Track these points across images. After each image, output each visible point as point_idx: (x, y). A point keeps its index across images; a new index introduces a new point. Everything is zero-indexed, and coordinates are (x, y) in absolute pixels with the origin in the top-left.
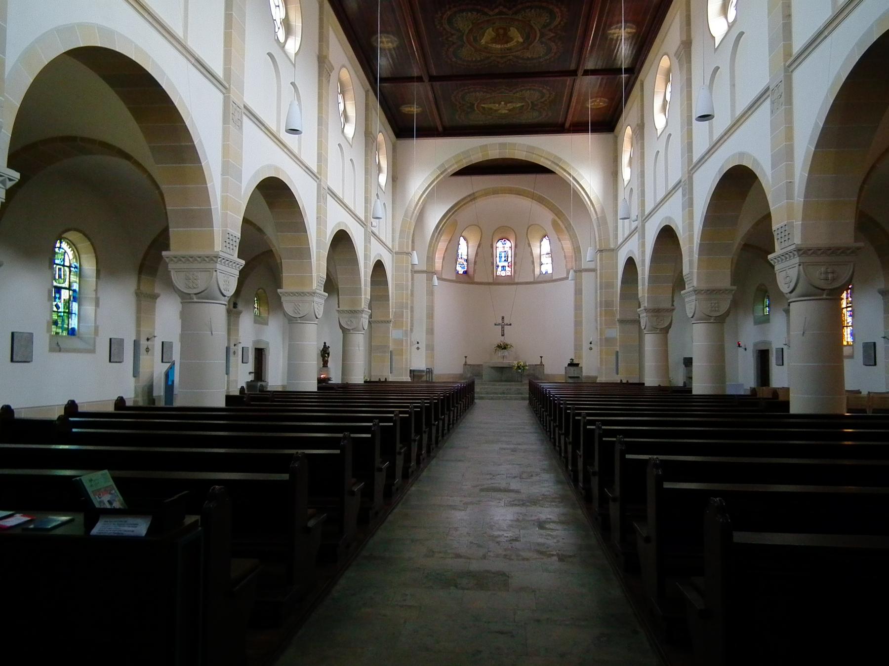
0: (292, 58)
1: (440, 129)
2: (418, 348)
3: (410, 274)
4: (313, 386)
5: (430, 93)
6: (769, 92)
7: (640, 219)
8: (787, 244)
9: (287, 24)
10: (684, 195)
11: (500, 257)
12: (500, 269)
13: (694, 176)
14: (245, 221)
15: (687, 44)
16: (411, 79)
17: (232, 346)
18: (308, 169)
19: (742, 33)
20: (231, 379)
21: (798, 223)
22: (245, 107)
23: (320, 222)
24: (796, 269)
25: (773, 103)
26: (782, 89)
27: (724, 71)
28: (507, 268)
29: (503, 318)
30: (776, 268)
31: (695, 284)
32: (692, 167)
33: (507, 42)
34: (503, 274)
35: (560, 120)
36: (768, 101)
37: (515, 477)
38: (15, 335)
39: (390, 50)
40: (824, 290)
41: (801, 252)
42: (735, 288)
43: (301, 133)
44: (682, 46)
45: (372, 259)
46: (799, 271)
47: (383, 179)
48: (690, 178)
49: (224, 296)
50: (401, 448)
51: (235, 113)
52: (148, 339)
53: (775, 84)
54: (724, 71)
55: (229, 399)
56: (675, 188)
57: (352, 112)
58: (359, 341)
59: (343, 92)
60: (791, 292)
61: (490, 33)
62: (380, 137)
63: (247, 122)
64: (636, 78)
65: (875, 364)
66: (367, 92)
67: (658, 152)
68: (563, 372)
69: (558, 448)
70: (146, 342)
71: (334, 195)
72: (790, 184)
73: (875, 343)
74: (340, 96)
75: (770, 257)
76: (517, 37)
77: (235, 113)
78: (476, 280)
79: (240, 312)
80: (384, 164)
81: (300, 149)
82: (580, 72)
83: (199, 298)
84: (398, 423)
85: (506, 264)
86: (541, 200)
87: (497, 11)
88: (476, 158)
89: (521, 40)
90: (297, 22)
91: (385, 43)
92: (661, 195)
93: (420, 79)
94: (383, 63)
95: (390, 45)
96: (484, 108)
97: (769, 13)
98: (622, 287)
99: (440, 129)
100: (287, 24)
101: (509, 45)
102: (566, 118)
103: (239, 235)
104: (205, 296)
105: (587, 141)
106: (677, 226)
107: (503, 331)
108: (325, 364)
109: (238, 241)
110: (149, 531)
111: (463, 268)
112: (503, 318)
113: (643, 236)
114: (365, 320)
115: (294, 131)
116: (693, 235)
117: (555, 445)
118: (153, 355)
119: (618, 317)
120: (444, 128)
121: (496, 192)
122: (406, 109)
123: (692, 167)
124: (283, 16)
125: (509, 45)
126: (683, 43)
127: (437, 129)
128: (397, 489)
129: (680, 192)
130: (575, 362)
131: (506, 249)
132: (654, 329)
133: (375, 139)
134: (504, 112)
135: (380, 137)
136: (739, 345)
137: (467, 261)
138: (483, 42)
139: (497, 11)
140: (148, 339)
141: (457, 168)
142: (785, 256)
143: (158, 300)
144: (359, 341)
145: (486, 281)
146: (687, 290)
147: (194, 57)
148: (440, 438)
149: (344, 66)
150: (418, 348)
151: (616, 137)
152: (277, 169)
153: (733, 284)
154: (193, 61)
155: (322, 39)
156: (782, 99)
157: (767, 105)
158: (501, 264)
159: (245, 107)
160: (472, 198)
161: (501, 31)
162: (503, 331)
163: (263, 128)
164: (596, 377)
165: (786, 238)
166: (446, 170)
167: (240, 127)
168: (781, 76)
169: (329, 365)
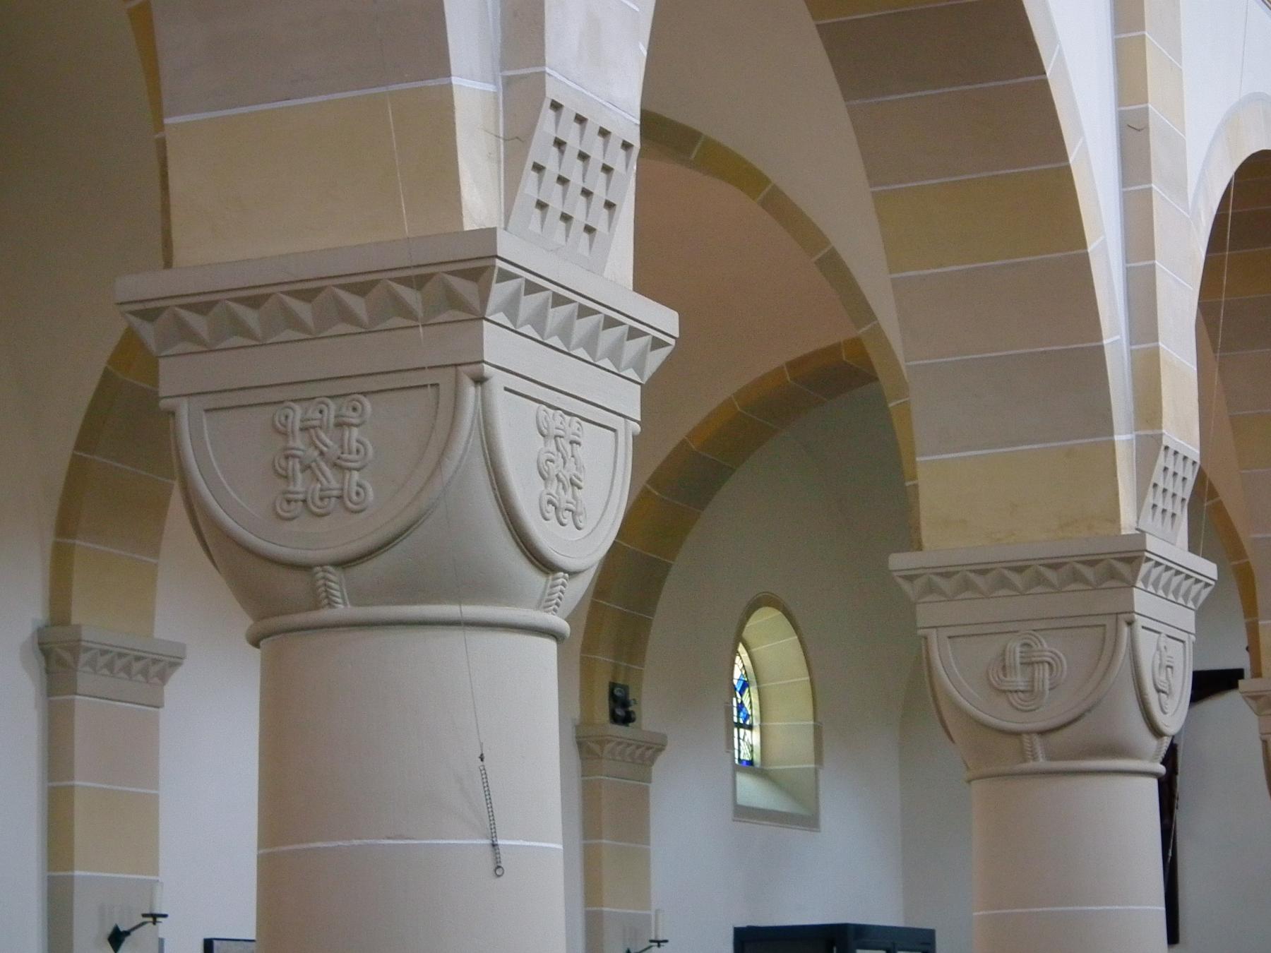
79: (653, 748)
104: (1083, 745)
143: (659, 768)
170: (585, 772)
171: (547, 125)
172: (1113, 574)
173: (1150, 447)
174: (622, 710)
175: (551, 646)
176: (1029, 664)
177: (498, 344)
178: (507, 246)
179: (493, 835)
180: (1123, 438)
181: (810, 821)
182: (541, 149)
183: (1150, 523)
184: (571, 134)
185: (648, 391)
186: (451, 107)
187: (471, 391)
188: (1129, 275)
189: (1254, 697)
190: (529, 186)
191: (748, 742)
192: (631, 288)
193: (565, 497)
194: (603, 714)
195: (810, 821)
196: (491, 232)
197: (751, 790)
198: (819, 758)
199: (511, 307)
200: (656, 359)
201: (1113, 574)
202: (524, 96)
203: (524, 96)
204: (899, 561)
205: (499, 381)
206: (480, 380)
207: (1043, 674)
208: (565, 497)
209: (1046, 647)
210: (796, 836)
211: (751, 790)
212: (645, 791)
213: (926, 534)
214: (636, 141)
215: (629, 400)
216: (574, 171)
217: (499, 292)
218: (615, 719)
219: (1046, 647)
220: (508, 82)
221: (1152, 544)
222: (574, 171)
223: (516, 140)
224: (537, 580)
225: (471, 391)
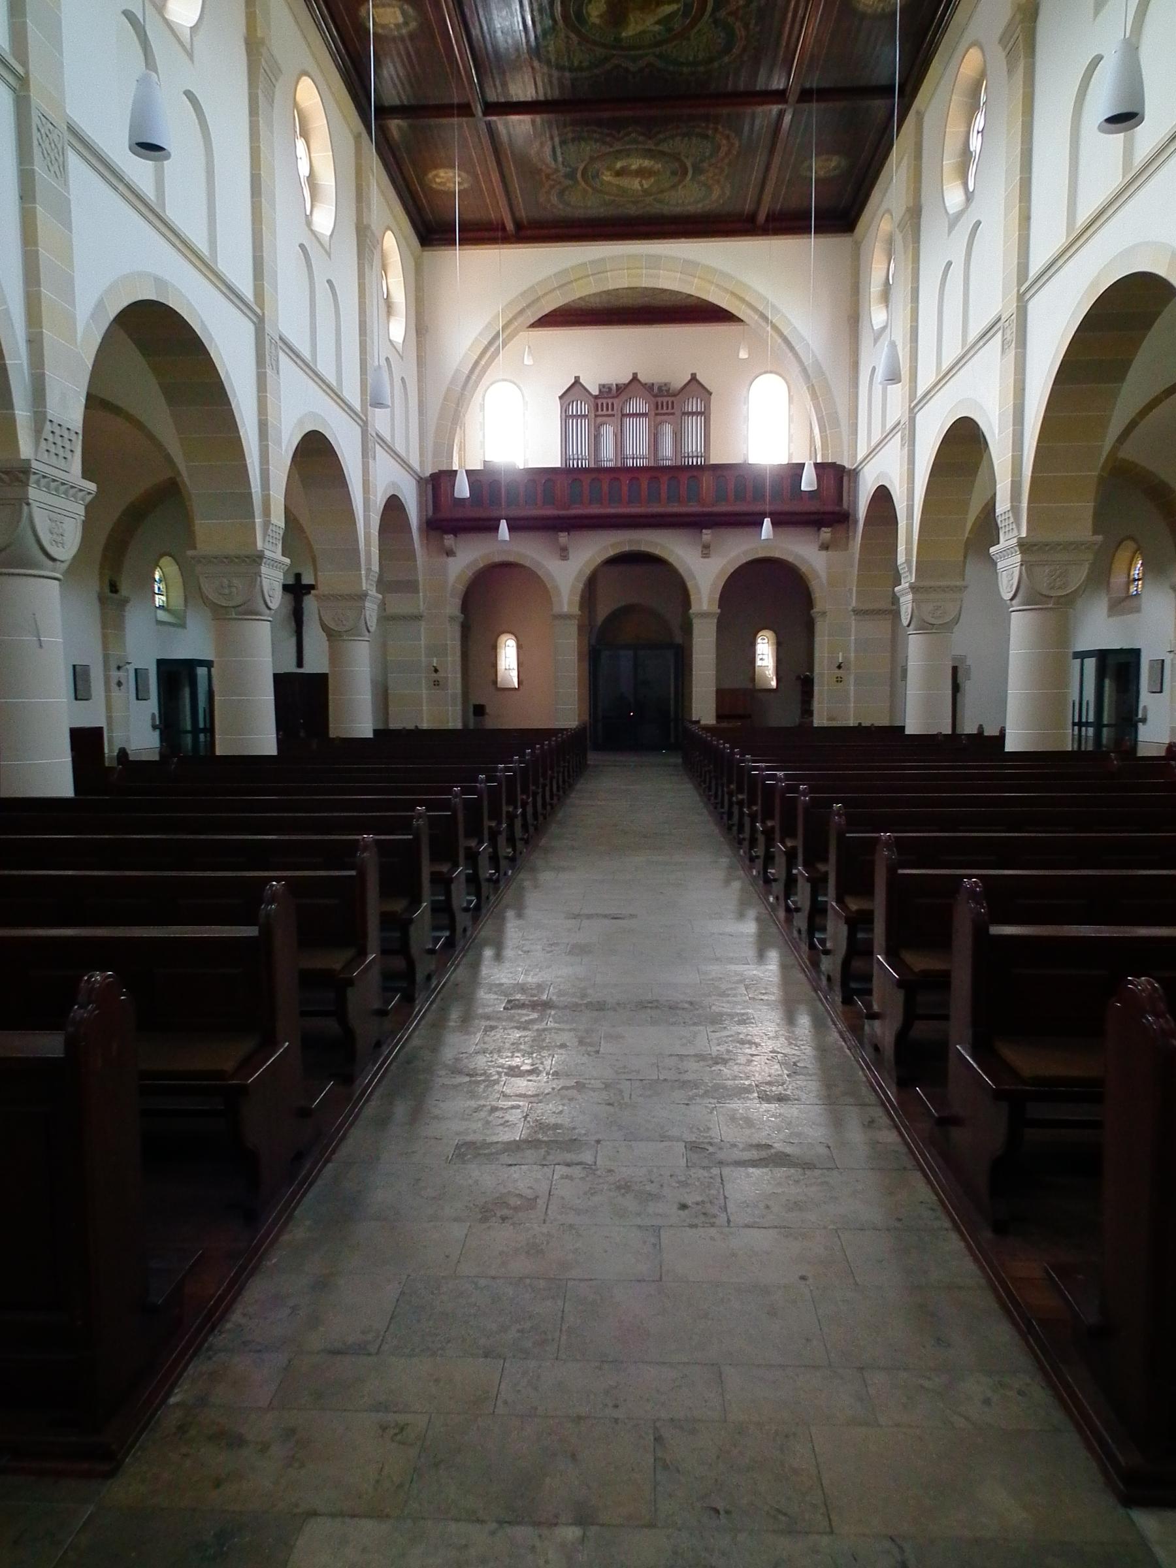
1: (510, 226)
4: (55, 777)
14: (90, 397)
15: (915, 213)
22: (281, 338)
23: (273, 411)
27: (957, 271)
30: (999, 565)
31: (854, 604)
32: (1026, 285)
35: (748, 207)
38: (78, 668)
42: (1100, 538)
43: (168, 157)
45: (379, 495)
47: (398, 329)
48: (912, 420)
49: (269, 609)
51: (267, 347)
52: (119, 668)
54: (957, 271)
56: (986, 335)
57: (327, 178)
59: (305, 135)
60: (1012, 599)
62: (390, 242)
66: (357, 138)
74: (300, 144)
75: (992, 550)
77: (267, 347)
79: (125, 602)
80: (399, 297)
81: (393, 436)
83: (240, 614)
92: (951, 353)
94: (389, 79)
99: (510, 226)
102: (759, 202)
103: (283, 526)
104: (247, 611)
105: (803, 252)
109: (282, 532)
113: (911, 441)
114: (371, 610)
115: (149, 148)
116: (913, 505)
119: (854, 604)
120: (519, 226)
123: (1026, 285)
126: (908, 210)
127: (504, 228)
132: (925, 627)
137: (793, 1074)
140: (119, 668)
142: (1006, 552)
143: (128, 608)
146: (1003, 543)
149: (388, 228)
151: (857, 246)
152: (159, 282)
153: (1095, 532)
155: (361, 196)
159: (281, 338)
163: (121, 187)
170: (102, 609)
171: (48, 426)
172: (254, 561)
173: (267, 524)
174: (114, 588)
175: (57, 582)
176: (229, 586)
177: (33, 493)
178: (34, 464)
179: (38, 636)
180: (258, 520)
181: (183, 626)
182: (46, 433)
183: (267, 546)
184: (57, 430)
185: (87, 507)
186: (15, 421)
187: (25, 507)
188: (261, 470)
189: (316, 596)
190: (43, 444)
191: (159, 600)
192: (80, 475)
193: (59, 539)
194: (107, 590)
195: (183, 626)
196: (29, 460)
197: (162, 616)
198: (186, 606)
199: (37, 482)
200: (89, 498)
201: (254, 561)
202: (40, 418)
203: (40, 418)
204: (190, 553)
205: (34, 505)
206: (28, 504)
207: (234, 590)
208: (59, 539)
209: (235, 581)
210: (179, 630)
211: (162, 616)
212: (124, 616)
213: (198, 546)
214: (80, 432)
215: (81, 510)
216: (59, 441)
217: (33, 478)
218: (112, 591)
219: (235, 581)
220: (35, 412)
221: (267, 553)
222: (59, 441)
223: (38, 431)
224: (50, 563)
225: (25, 507)
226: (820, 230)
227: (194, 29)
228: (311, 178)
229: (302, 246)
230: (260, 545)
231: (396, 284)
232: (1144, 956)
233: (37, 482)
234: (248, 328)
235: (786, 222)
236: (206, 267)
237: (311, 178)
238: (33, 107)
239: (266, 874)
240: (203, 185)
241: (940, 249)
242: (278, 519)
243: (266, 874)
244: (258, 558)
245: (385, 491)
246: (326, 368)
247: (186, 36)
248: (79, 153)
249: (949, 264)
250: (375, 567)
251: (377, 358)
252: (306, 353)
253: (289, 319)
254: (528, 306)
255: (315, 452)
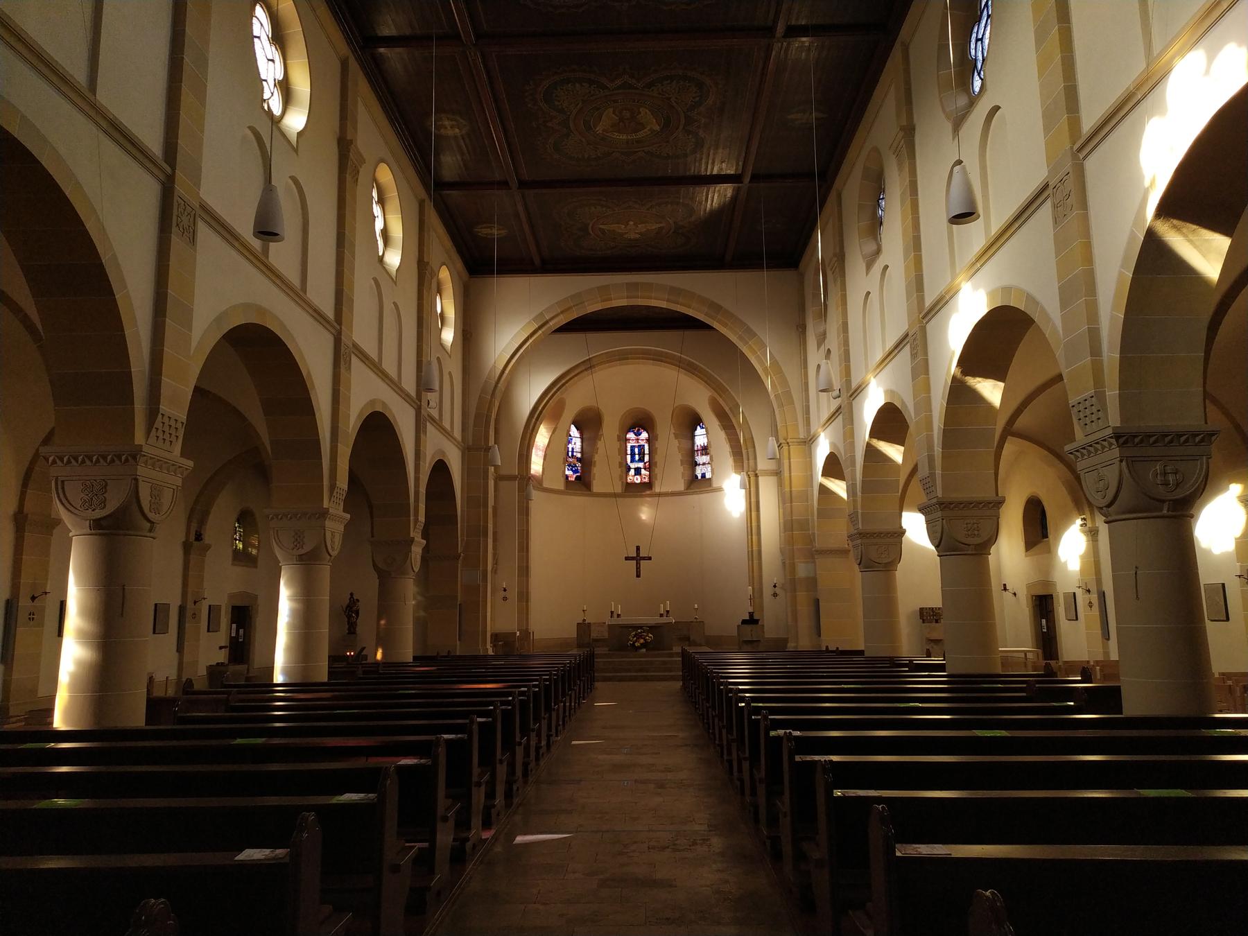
0: (294, 139)
1: (537, 261)
2: (505, 599)
3: (491, 483)
5: (521, 209)
6: (1049, 191)
7: (845, 395)
8: (1094, 427)
9: (285, 87)
10: (914, 356)
11: (633, 455)
12: (632, 472)
13: (928, 326)
14: (197, 390)
16: (491, 185)
17: (190, 605)
18: (318, 315)
19: (996, 109)
20: (185, 659)
21: (1112, 393)
23: (343, 399)
24: (1116, 468)
25: (1055, 206)
26: (1070, 184)
28: (643, 471)
29: (638, 548)
33: (635, 131)
34: (638, 480)
36: (1048, 204)
37: (664, 848)
39: (455, 137)
40: (1163, 501)
41: (1121, 440)
44: (901, 134)
46: (1121, 471)
50: (448, 809)
51: (341, 354)
52: (33, 598)
53: (1058, 177)
54: (874, 297)
55: (155, 706)
58: (410, 593)
61: (608, 117)
62: (444, 274)
63: (203, 230)
64: (829, 188)
65: (1228, 619)
67: (868, 293)
68: (735, 633)
69: (738, 783)
70: (29, 603)
71: (364, 357)
72: (1094, 334)
73: (1223, 585)
76: (653, 124)
78: (546, 485)
82: (780, 29)
84: (442, 759)
85: (641, 465)
86: (691, 369)
87: (618, 82)
88: (594, 306)
89: (657, 128)
90: (302, 84)
91: (450, 128)
93: (504, 184)
94: (450, 164)
95: (457, 130)
96: (603, 231)
97: (1040, 74)
98: (819, 500)
99: (537, 261)
100: (285, 87)
101: (641, 134)
106: (903, 402)
107: (638, 568)
108: (352, 629)
110: (639, 519)
111: (575, 472)
112: (638, 548)
116: (931, 416)
117: (731, 772)
118: (41, 624)
121: (623, 357)
122: (483, 231)
124: (280, 76)
125: (641, 134)
128: (439, 894)
129: (907, 349)
130: (756, 617)
131: (642, 443)
133: (435, 274)
134: (633, 236)
135: (444, 274)
136: (1005, 589)
138: (599, 129)
139: (618, 82)
140: (33, 598)
141: (562, 320)
144: (410, 593)
145: (611, 490)
147: (105, 118)
148: (532, 765)
149: (382, 161)
150: (505, 599)
152: (261, 311)
154: (104, 124)
156: (1073, 200)
157: (1045, 212)
158: (633, 466)
160: (588, 366)
161: (627, 114)
162: (638, 568)
163: (236, 244)
164: (786, 641)
165: (1094, 417)
166: (547, 322)
167: (193, 240)
168: (1068, 166)
169: (358, 629)
182: (158, 424)
200: (185, 473)
226: (770, 267)
227: (300, 134)
228: (385, 232)
229: (375, 280)
230: (326, 505)
231: (446, 305)
232: (310, 808)
233: (146, 463)
234: (327, 340)
235: (744, 260)
236: (298, 295)
237: (385, 232)
238: (176, 198)
239: (762, 741)
240: (179, 582)
241: (860, 281)
242: (343, 483)
243: (762, 741)
244: (324, 514)
245: (433, 457)
246: (389, 366)
247: (294, 139)
248: (206, 222)
249: (868, 293)
250: (422, 518)
251: (432, 356)
252: (373, 354)
253: (361, 332)
254: (540, 328)
255: (377, 427)
